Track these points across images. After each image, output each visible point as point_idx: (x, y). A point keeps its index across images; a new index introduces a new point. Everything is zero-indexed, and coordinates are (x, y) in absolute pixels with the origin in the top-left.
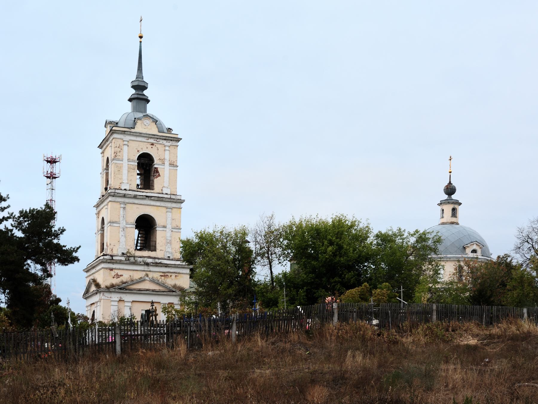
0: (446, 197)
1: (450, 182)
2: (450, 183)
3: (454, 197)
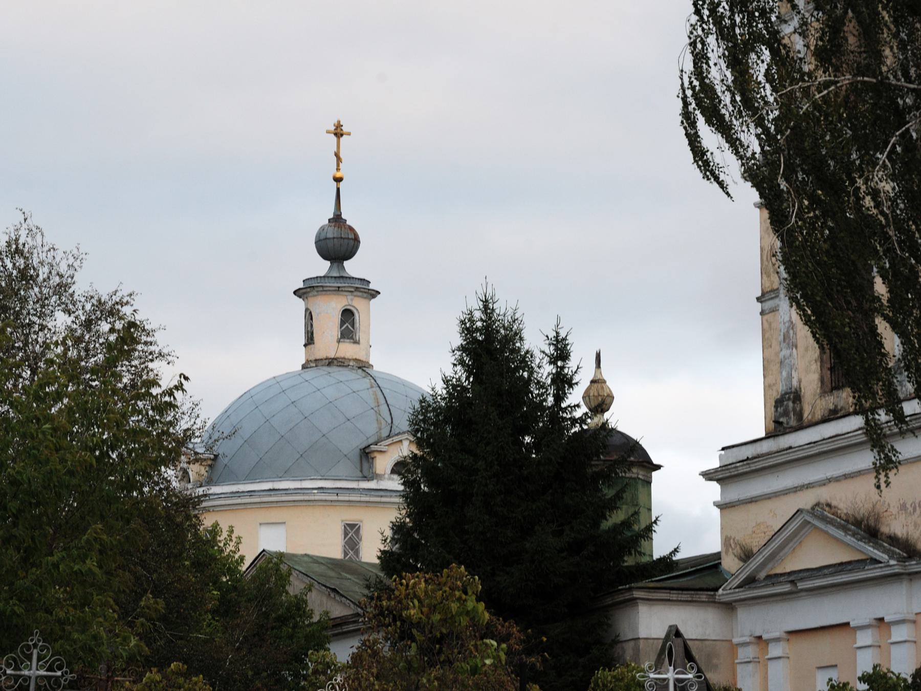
0: (322, 267)
1: (337, 219)
2: (337, 219)
3: (352, 267)
